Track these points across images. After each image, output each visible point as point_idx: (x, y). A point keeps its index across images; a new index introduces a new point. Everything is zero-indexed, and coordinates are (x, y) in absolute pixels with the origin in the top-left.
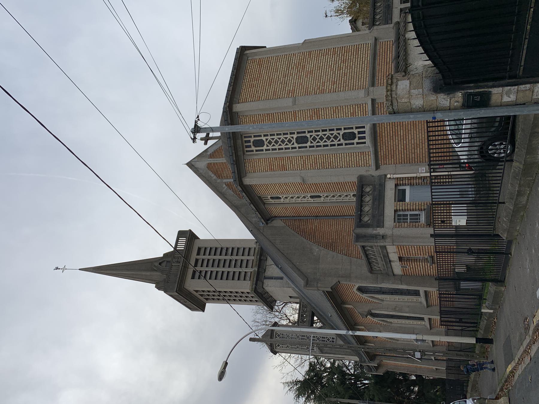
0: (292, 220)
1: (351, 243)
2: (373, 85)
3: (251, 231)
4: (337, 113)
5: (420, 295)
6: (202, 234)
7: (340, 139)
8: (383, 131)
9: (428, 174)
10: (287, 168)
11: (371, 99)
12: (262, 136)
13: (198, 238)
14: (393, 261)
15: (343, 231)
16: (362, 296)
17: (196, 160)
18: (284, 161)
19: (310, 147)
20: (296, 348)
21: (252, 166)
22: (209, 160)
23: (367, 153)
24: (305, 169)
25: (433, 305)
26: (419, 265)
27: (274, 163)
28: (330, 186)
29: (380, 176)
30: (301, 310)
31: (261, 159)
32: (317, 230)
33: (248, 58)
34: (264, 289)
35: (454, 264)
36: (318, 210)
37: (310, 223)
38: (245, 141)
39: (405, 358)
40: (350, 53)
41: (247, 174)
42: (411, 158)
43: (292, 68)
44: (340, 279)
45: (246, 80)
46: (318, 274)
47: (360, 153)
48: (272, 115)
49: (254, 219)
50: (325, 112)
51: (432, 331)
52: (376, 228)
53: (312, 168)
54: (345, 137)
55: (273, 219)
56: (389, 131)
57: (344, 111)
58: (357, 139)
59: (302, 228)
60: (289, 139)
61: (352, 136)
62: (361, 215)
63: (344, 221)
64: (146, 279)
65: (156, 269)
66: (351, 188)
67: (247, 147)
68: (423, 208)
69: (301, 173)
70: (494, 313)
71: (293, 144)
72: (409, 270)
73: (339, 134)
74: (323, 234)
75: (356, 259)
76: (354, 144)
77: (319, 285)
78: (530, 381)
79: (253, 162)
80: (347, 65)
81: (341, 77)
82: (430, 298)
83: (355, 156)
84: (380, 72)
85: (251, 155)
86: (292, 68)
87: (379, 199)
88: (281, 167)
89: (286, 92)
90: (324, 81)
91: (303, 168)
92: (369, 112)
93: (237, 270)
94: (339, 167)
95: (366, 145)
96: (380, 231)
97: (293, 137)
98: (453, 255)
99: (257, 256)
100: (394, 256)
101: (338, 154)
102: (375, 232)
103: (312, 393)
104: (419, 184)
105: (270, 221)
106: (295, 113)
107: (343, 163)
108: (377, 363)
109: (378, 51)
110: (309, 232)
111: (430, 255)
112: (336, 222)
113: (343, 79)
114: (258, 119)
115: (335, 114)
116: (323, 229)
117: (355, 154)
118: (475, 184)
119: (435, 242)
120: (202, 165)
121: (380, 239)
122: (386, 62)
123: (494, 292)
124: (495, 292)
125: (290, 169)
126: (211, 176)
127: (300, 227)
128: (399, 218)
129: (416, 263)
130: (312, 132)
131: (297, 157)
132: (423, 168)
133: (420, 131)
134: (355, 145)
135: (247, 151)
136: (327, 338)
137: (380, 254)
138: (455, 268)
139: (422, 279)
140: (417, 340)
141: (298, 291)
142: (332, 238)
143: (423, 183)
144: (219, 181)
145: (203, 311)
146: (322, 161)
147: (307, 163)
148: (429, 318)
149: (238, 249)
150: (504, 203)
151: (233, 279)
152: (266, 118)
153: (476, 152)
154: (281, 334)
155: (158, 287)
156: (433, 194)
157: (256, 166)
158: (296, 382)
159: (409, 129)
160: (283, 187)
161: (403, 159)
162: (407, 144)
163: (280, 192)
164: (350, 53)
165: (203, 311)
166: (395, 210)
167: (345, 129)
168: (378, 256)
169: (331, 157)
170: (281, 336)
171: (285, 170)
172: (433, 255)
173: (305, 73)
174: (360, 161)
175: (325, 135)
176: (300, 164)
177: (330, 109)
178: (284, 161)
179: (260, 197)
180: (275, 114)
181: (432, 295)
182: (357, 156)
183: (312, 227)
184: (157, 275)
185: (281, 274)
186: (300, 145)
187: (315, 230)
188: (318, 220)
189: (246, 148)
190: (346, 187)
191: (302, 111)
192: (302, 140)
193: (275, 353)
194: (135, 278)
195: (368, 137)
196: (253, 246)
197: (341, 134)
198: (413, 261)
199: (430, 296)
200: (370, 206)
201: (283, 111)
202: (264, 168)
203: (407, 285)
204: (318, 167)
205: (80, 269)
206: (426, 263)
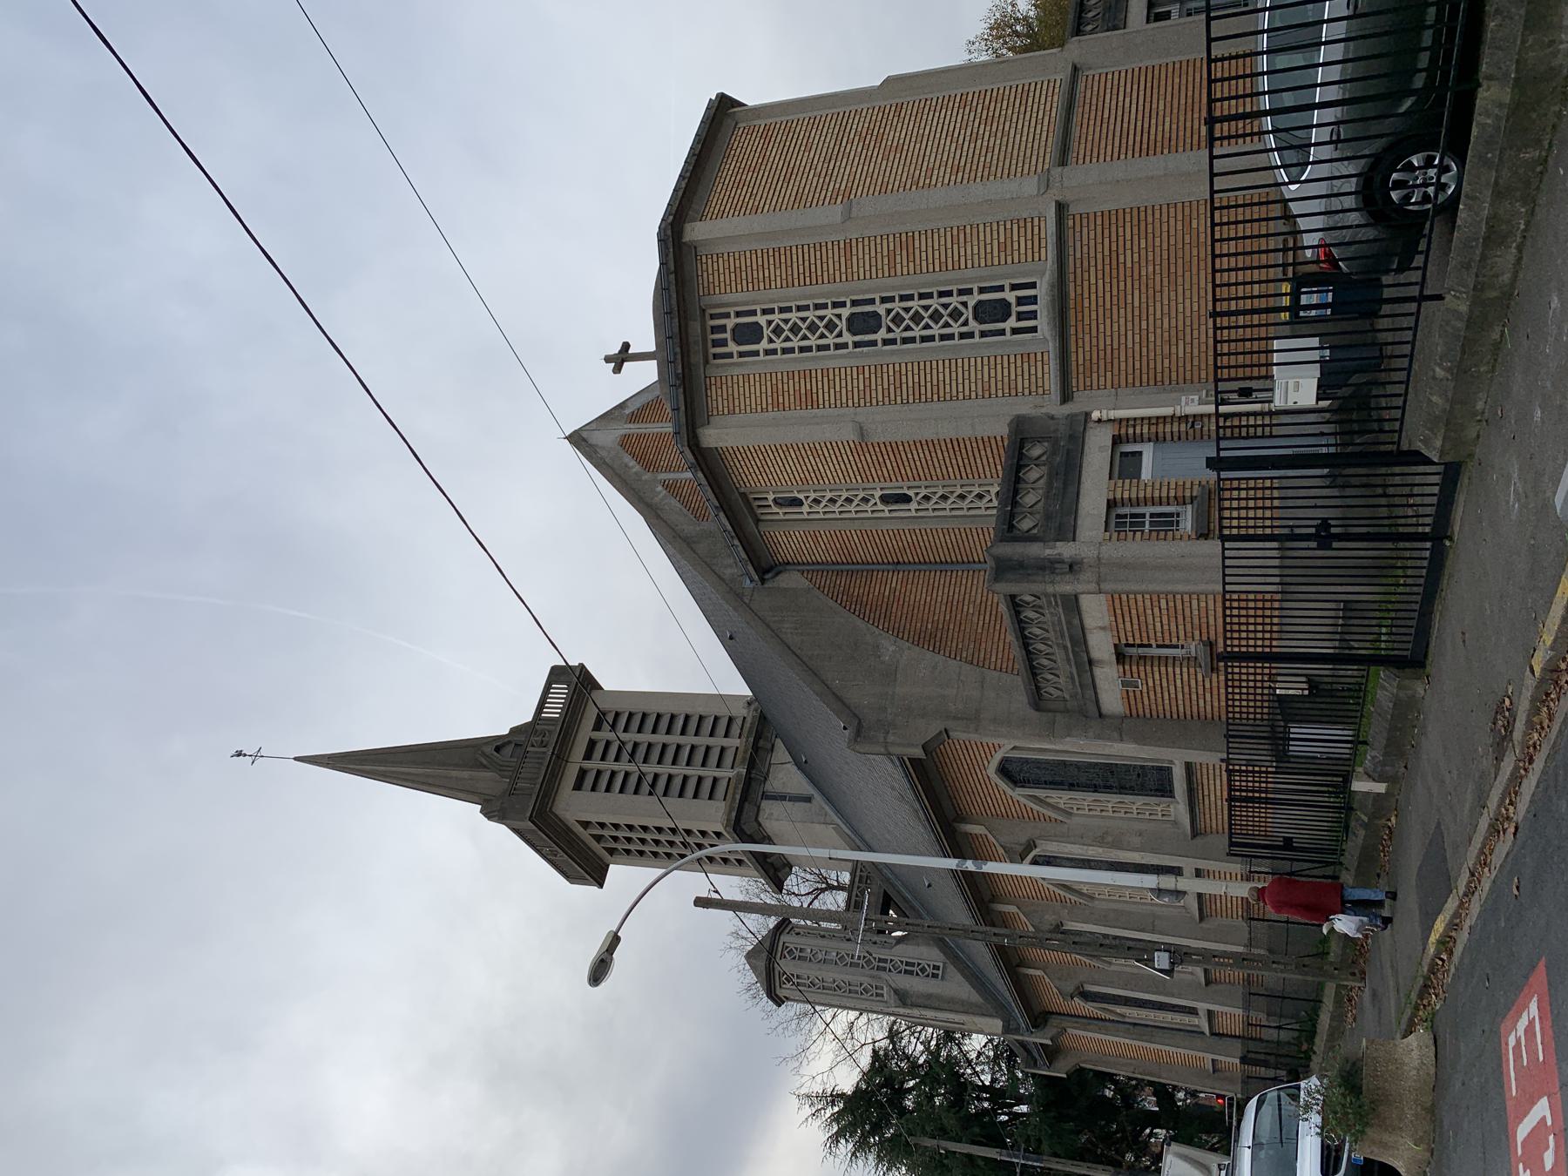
0: (830, 573)
1: (985, 632)
2: (1063, 162)
3: (730, 641)
4: (962, 245)
5: (1173, 797)
6: (611, 679)
7: (967, 320)
8: (1086, 295)
9: (1211, 409)
10: (821, 401)
11: (1057, 202)
12: (759, 312)
13: (602, 689)
14: (1100, 662)
15: (966, 603)
16: (1013, 794)
17: (594, 426)
18: (814, 380)
19: (886, 342)
20: (835, 990)
21: (725, 397)
22: (626, 426)
23: (1039, 358)
24: (868, 404)
25: (1208, 830)
26: (1171, 674)
27: (786, 386)
28: (935, 460)
29: (1071, 417)
30: (855, 889)
31: (752, 376)
32: (896, 599)
33: (737, 124)
34: (760, 825)
35: (1274, 671)
36: (900, 544)
37: (879, 581)
38: (712, 327)
39: (1127, 1026)
40: (1005, 103)
41: (711, 419)
42: (1159, 369)
43: (850, 141)
44: (950, 724)
45: (727, 173)
46: (889, 711)
47: (1019, 357)
48: (788, 253)
49: (729, 571)
50: (930, 240)
51: (1203, 925)
52: (1051, 544)
53: (887, 399)
54: (982, 312)
55: (781, 568)
56: (1100, 294)
57: (982, 238)
58: (1013, 317)
59: (856, 594)
60: (831, 320)
61: (1000, 311)
62: (1012, 516)
63: (970, 578)
64: (461, 791)
65: (485, 762)
66: (992, 465)
67: (716, 343)
68: (1188, 494)
69: (855, 414)
70: (1388, 794)
71: (840, 335)
72: (1145, 695)
73: (965, 304)
74: (911, 608)
75: (996, 674)
76: (1004, 335)
77: (891, 738)
78: (1516, 892)
79: (730, 384)
80: (994, 129)
81: (976, 157)
82: (1201, 805)
83: (1006, 365)
84: (1083, 141)
85: (723, 365)
86: (850, 141)
87: (1068, 471)
88: (803, 399)
89: (829, 194)
90: (931, 165)
91: (862, 401)
92: (1049, 241)
93: (693, 772)
94: (961, 397)
95: (1039, 335)
96: (1065, 550)
97: (839, 316)
98: (1270, 668)
99: (748, 737)
100: (1101, 645)
101: (960, 361)
102: (1048, 552)
103: (872, 1133)
104: (1179, 438)
105: (770, 575)
106: (848, 245)
107: (973, 385)
108: (1050, 1035)
109: (1079, 96)
110: (874, 603)
111: (1205, 638)
112: (948, 578)
113: (982, 159)
114: (749, 264)
115: (955, 246)
116: (913, 597)
117: (1005, 358)
118: (1340, 445)
119: (1228, 748)
120: (607, 439)
121: (1062, 574)
122: (1099, 118)
123: (1391, 705)
124: (1397, 703)
125: (827, 403)
126: (626, 466)
127: (851, 590)
128: (1120, 518)
129: (1163, 669)
130: (891, 299)
131: (849, 370)
132: (1191, 397)
133: (1188, 293)
134: (1008, 336)
135: (715, 356)
136: (919, 964)
137: (1063, 636)
138: (1275, 688)
139: (1176, 727)
140: (1159, 892)
141: (850, 833)
142: (936, 618)
143: (1191, 431)
144: (647, 476)
145: (601, 885)
146: (916, 380)
147: (873, 387)
148: (1208, 1011)
149: (701, 718)
150: (1439, 297)
151: (681, 795)
152: (772, 262)
153: (1349, 202)
154: (796, 949)
155: (489, 814)
156: (1228, 562)
157: (736, 396)
158: (831, 1095)
159: (1158, 288)
160: (806, 460)
161: (1137, 372)
162: (1151, 329)
163: (798, 479)
164: (1005, 103)
165: (601, 885)
166: (1108, 501)
167: (982, 290)
168: (1058, 645)
169: (941, 370)
170: (797, 954)
171: (815, 406)
172: (1212, 637)
173: (881, 151)
174: (1020, 378)
175: (926, 308)
176: (856, 390)
177: (942, 234)
178: (814, 380)
179: (744, 495)
180: (794, 249)
181: (1206, 793)
182: (1013, 366)
183: (882, 591)
184: (488, 779)
185: (808, 789)
186: (858, 338)
187: (891, 599)
188: (901, 573)
189: (714, 346)
190: (978, 461)
191: (866, 240)
192: (863, 323)
193: (779, 1002)
194: (434, 785)
195: (1045, 313)
196: (740, 711)
197: (971, 304)
198: (1156, 663)
199: (1201, 797)
200: (1041, 491)
201: (817, 240)
202: (759, 402)
203: (1137, 743)
204: (905, 397)
205: (295, 759)
206: (1192, 670)
